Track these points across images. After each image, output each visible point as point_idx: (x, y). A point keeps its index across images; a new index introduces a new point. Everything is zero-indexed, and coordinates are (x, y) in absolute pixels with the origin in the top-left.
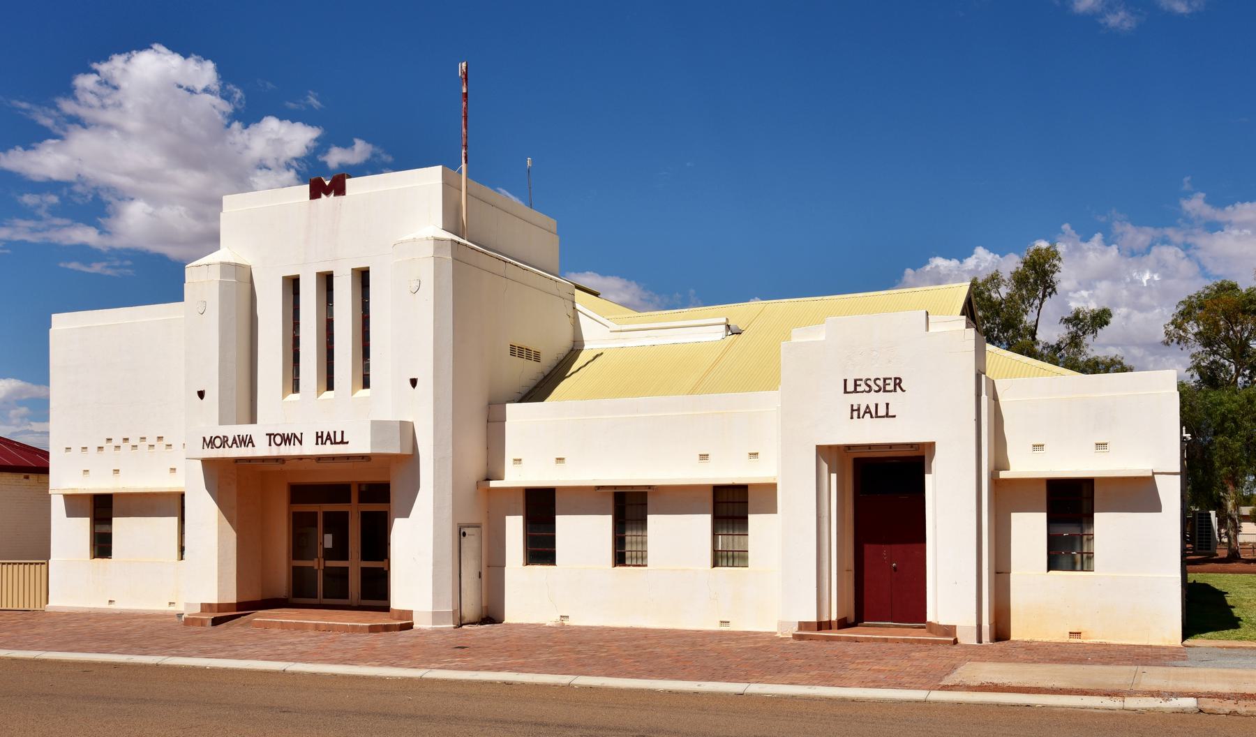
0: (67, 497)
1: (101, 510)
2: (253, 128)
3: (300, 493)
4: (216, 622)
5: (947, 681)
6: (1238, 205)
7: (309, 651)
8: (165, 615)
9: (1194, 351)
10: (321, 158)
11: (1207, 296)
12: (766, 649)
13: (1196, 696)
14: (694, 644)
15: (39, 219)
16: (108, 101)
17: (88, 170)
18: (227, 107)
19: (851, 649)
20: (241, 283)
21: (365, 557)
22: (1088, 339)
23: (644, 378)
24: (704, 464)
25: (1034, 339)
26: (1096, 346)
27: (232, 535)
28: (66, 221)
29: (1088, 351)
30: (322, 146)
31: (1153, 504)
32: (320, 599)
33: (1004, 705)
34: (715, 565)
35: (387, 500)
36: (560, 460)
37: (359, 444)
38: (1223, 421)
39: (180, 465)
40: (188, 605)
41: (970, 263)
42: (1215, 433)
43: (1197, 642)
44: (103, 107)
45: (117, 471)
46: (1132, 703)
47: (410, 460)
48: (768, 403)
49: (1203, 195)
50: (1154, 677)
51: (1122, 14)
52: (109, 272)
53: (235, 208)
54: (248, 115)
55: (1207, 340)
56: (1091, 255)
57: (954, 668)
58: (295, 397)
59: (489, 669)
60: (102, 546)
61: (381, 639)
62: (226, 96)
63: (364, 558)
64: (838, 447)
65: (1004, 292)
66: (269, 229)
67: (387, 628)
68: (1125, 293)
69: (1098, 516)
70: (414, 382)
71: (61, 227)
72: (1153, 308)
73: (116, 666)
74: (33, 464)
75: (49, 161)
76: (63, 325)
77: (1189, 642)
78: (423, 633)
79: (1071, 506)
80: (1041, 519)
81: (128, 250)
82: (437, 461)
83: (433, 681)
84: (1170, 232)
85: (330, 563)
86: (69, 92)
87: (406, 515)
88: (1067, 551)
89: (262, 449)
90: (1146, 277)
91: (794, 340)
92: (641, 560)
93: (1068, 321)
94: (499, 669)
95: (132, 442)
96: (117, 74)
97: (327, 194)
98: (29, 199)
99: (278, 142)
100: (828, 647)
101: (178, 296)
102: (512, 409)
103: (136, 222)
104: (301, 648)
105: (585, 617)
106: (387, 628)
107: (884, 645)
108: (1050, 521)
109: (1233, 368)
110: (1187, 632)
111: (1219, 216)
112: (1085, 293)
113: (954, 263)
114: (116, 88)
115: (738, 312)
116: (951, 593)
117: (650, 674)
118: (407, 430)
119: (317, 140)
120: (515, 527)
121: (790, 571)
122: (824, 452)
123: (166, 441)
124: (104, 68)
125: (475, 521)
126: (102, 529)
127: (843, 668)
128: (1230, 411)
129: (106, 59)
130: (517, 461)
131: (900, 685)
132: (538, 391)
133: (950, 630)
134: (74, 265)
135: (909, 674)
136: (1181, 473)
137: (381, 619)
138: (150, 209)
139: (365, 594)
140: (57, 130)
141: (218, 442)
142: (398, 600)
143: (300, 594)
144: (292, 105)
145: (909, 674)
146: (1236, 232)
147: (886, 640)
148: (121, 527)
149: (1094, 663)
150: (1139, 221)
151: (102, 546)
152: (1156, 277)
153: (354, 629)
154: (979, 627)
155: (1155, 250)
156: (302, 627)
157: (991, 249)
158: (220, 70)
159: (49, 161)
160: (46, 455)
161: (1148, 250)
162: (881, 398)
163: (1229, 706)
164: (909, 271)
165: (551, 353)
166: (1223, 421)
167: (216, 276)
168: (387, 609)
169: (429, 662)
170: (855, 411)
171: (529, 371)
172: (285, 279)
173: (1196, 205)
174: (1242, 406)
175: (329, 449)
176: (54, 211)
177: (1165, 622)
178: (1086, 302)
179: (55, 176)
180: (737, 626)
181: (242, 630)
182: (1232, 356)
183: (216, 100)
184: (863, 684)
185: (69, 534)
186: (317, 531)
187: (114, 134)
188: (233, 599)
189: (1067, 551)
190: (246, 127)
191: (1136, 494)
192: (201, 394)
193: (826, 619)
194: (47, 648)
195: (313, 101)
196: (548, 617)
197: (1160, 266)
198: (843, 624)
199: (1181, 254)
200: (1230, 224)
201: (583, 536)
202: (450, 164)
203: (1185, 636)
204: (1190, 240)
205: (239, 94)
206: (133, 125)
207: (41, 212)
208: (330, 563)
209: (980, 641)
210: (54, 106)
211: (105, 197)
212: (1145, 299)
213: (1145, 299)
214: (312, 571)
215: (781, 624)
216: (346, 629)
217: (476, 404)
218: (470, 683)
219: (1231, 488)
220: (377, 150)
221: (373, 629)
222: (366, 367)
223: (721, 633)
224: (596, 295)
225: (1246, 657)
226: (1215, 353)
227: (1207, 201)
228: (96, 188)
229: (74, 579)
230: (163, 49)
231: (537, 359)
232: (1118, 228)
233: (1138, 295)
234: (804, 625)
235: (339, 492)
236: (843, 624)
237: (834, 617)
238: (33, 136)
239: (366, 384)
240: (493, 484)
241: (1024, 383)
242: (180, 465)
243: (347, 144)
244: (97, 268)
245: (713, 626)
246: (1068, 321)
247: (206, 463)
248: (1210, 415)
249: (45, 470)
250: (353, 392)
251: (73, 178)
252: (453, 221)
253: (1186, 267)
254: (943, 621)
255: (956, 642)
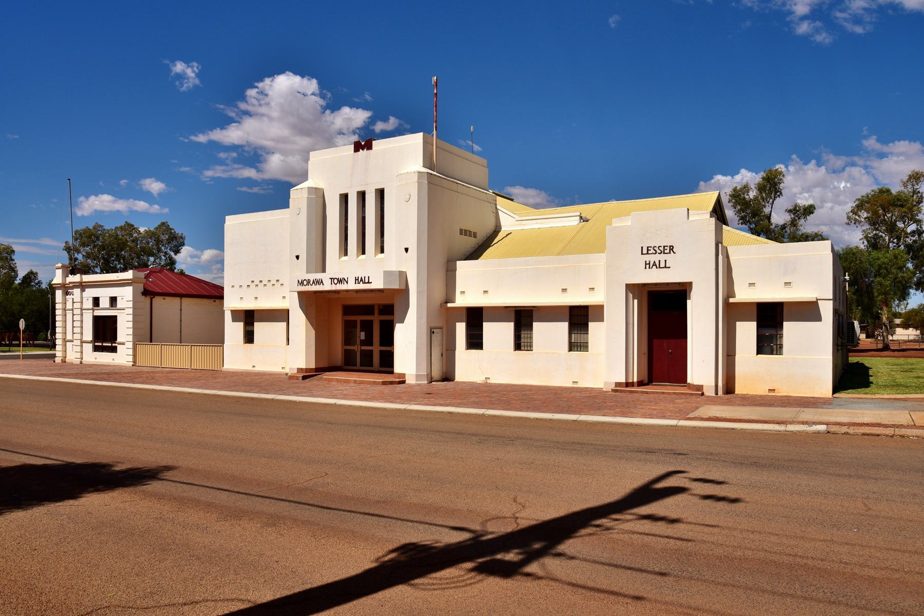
0: (232, 311)
1: (249, 318)
2: (336, 113)
3: (348, 310)
4: (304, 378)
5: (691, 415)
6: (897, 143)
7: (351, 394)
8: (280, 374)
9: (864, 228)
10: (372, 128)
11: (873, 196)
12: (595, 397)
13: (827, 424)
14: (556, 393)
15: (227, 165)
16: (262, 102)
17: (252, 139)
18: (322, 102)
19: (643, 397)
20: (318, 197)
21: (381, 345)
22: (802, 221)
23: (536, 246)
24: (564, 294)
25: (769, 221)
26: (807, 226)
27: (313, 332)
28: (240, 166)
29: (802, 228)
30: (372, 121)
31: (817, 317)
32: (358, 367)
33: (720, 429)
34: (570, 350)
35: (392, 314)
36: (486, 292)
37: (378, 283)
38: (880, 269)
39: (287, 295)
40: (291, 369)
41: (738, 178)
42: (875, 276)
43: (842, 395)
44: (260, 105)
45: (256, 298)
46: (791, 428)
47: (404, 292)
48: (599, 260)
49: (875, 137)
50: (808, 414)
51: (824, 35)
52: (262, 192)
53: (317, 158)
54: (334, 106)
55: (873, 222)
56: (810, 172)
57: (697, 408)
58: (363, 257)
59: (441, 405)
60: (249, 337)
61: (387, 389)
62: (322, 96)
63: (381, 345)
64: (638, 285)
65: (752, 194)
66: (332, 170)
67: (392, 383)
68: (830, 194)
69: (786, 325)
70: (407, 250)
71: (238, 169)
72: (847, 203)
73: (252, 399)
74: (215, 293)
75: (233, 135)
76: (233, 222)
77: (836, 395)
78: (411, 386)
79: (771, 319)
80: (753, 325)
81: (271, 180)
82: (419, 293)
83: (411, 411)
84: (856, 159)
85: (364, 348)
86: (243, 98)
87: (402, 321)
88: (768, 343)
89: (327, 286)
90: (843, 185)
91: (614, 225)
92: (530, 348)
93: (790, 211)
94: (447, 405)
95: (264, 283)
96: (267, 88)
97: (363, 149)
98: (222, 155)
99: (349, 119)
100: (630, 396)
101: (288, 207)
102: (461, 265)
103: (275, 164)
104: (345, 392)
105: (499, 378)
106: (392, 383)
107: (662, 396)
108: (759, 327)
109: (887, 238)
110: (835, 390)
111: (885, 149)
112: (806, 195)
113: (729, 178)
114: (267, 95)
115: (587, 209)
116: (701, 367)
117: (528, 409)
118: (403, 276)
119: (369, 118)
120: (461, 329)
121: (610, 356)
122: (630, 288)
123: (281, 282)
124: (260, 85)
125: (439, 325)
126: (249, 328)
127: (635, 408)
128: (884, 263)
129: (262, 80)
130: (463, 292)
131: (664, 417)
132: (475, 254)
133: (700, 388)
134: (244, 189)
135: (671, 411)
136: (834, 299)
137: (389, 378)
138: (282, 158)
139: (382, 365)
140: (237, 119)
141: (305, 283)
142: (398, 369)
143: (348, 364)
144: (356, 100)
145: (671, 411)
146: (895, 159)
147: (663, 393)
148: (258, 327)
149: (778, 406)
150: (838, 153)
151: (249, 337)
152: (848, 185)
153: (374, 383)
154: (717, 386)
155: (847, 169)
156: (347, 382)
157: (750, 169)
158: (319, 83)
159: (233, 135)
160: (222, 288)
161: (843, 170)
162: (662, 257)
163: (844, 429)
164: (702, 183)
165: (483, 232)
166: (880, 269)
167: (305, 195)
168: (392, 372)
169: (411, 401)
170: (647, 264)
171: (470, 243)
172: (341, 195)
173: (871, 143)
174: (891, 261)
175: (362, 286)
176: (235, 161)
177: (823, 385)
178: (807, 200)
179: (236, 142)
180: (583, 384)
181: (317, 383)
182: (887, 230)
183: (317, 99)
184: (644, 416)
185: (234, 330)
186: (356, 329)
187: (265, 119)
188: (313, 366)
189: (768, 343)
190: (332, 112)
191: (807, 311)
192: (297, 257)
193: (631, 381)
194: (220, 389)
195: (368, 97)
196: (479, 379)
197: (850, 179)
198: (640, 383)
199: (863, 171)
200: (892, 153)
201: (498, 334)
202: (427, 132)
203: (834, 392)
204: (868, 163)
205: (329, 95)
206: (275, 114)
207: (228, 161)
208: (364, 348)
209: (717, 394)
210: (236, 106)
211: (260, 152)
212: (842, 198)
213: (842, 198)
214: (354, 352)
215: (606, 383)
216: (370, 383)
217: (441, 260)
218: (430, 412)
219: (885, 308)
220: (402, 122)
221: (384, 383)
222: (382, 242)
223: (573, 388)
224: (512, 200)
225: (866, 403)
226: (877, 229)
227: (878, 140)
228: (255, 148)
229: (236, 356)
230: (291, 74)
231: (475, 236)
232: (825, 157)
233: (838, 196)
234: (618, 384)
235: (368, 309)
236: (640, 383)
237: (635, 380)
238: (225, 122)
239: (382, 251)
240: (449, 305)
241: (747, 249)
242: (287, 295)
243: (385, 120)
244: (255, 190)
245: (569, 384)
246: (790, 211)
247: (300, 294)
248: (872, 265)
249: (222, 298)
250: (376, 255)
251: (244, 143)
252: (428, 162)
253: (866, 179)
254: (696, 382)
255: (703, 394)
